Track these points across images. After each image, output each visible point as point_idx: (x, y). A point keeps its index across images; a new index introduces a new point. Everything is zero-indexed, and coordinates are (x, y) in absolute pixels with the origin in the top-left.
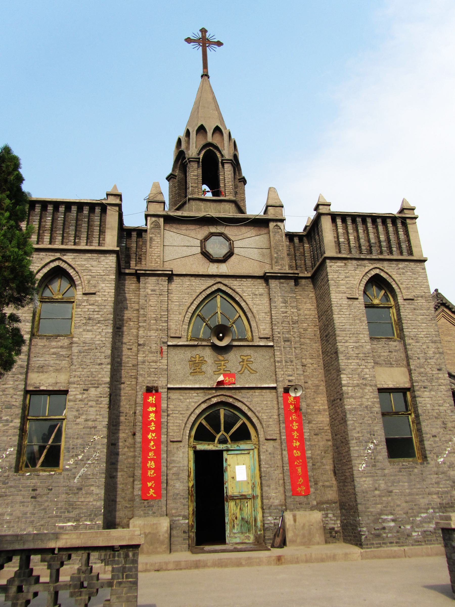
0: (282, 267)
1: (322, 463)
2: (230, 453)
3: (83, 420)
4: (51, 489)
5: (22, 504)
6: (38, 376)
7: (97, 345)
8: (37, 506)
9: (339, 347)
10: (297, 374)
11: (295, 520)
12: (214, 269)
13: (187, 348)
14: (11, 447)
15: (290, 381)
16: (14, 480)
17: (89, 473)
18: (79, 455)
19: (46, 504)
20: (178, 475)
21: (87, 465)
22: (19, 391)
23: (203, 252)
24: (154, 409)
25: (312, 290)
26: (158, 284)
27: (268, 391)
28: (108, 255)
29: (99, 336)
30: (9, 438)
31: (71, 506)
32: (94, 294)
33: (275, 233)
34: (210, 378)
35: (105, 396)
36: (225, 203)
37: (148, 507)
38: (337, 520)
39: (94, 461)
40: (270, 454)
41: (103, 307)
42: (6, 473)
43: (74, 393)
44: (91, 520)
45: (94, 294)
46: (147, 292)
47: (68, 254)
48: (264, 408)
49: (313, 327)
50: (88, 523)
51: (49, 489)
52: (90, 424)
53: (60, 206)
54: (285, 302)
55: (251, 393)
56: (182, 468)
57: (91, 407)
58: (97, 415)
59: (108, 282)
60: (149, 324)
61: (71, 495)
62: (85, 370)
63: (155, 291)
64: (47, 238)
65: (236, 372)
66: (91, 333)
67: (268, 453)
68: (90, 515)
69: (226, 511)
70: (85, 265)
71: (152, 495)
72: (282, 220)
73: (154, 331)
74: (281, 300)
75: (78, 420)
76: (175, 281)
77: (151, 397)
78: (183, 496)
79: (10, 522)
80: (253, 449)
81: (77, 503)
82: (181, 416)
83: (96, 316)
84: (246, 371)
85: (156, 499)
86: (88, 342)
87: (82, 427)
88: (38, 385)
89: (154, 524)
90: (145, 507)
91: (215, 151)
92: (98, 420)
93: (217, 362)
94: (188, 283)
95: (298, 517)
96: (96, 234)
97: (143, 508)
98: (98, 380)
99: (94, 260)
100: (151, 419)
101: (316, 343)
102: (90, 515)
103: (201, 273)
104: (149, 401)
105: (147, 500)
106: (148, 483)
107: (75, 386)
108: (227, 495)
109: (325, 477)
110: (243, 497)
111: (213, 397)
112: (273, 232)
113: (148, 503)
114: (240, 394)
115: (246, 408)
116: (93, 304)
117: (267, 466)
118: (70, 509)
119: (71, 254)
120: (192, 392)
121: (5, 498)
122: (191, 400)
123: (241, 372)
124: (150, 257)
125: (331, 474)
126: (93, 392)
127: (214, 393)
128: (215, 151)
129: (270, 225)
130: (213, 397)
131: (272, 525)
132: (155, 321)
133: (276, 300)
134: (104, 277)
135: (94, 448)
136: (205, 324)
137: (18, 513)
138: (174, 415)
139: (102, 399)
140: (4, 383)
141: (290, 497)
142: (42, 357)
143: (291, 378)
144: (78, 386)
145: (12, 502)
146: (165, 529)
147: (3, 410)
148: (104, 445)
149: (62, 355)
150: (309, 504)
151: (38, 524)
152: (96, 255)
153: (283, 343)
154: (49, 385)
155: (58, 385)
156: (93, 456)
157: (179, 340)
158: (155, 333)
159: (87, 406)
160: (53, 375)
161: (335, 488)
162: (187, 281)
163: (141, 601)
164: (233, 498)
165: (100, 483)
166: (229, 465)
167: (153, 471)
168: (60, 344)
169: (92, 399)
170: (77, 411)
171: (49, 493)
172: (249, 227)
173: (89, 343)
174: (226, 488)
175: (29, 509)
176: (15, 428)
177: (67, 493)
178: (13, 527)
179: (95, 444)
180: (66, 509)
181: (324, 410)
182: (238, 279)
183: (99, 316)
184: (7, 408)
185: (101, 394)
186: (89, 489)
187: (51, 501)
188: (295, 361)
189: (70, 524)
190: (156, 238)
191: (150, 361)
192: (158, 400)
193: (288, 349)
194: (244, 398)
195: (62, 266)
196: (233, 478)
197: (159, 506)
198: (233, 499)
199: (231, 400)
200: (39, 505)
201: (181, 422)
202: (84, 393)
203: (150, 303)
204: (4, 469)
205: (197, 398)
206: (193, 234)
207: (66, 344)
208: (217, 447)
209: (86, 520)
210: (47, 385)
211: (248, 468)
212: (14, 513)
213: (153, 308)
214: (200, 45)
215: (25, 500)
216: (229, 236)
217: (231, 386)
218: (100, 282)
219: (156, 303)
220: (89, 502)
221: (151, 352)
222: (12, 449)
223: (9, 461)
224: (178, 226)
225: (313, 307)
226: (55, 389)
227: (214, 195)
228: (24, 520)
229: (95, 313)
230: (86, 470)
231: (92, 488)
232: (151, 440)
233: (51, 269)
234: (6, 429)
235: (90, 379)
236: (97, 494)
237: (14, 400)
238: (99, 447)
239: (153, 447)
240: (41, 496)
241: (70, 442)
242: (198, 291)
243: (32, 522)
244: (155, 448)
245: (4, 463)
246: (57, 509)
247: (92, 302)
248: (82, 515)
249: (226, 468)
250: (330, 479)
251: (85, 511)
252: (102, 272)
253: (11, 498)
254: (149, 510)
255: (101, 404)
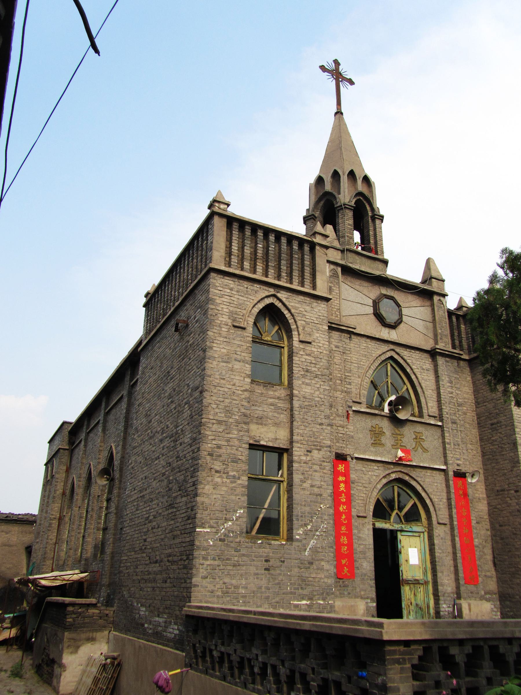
0: (446, 345)
1: (483, 552)
2: (403, 533)
3: (308, 486)
4: (283, 562)
5: (255, 577)
6: (258, 429)
7: (316, 402)
8: (271, 580)
9: (518, 439)
10: (464, 459)
11: (470, 610)
12: (385, 333)
13: (367, 416)
14: (241, 508)
15: (458, 465)
16: (246, 547)
17: (318, 546)
18: (309, 525)
19: (280, 578)
20: (365, 554)
21: (315, 537)
22: (244, 443)
23: (377, 313)
24: (344, 479)
25: (469, 374)
26: (341, 340)
27: (437, 472)
28: (319, 302)
29: (318, 393)
30: (238, 497)
31: (304, 582)
32: (310, 343)
33: (439, 307)
34: (389, 452)
35: (328, 460)
36: (379, 263)
37: (344, 587)
38: (498, 611)
39: (322, 533)
40: (442, 538)
41: (319, 360)
42: (237, 538)
43: (299, 453)
44: (324, 600)
45: (310, 343)
46: (331, 347)
47: (282, 292)
48: (436, 490)
49: (471, 412)
50: (322, 602)
51: (281, 561)
52: (316, 490)
53: (270, 234)
54: (451, 382)
55: (423, 473)
56: (367, 546)
57: (316, 471)
58: (321, 481)
59: (321, 332)
60: (335, 383)
61: (303, 570)
62: (307, 429)
63: (338, 348)
64: (260, 268)
65: (411, 448)
66: (309, 388)
67: (440, 537)
68: (323, 593)
69: (402, 595)
70: (299, 308)
71: (346, 574)
72: (444, 295)
73: (340, 393)
74: (447, 379)
75: (305, 485)
76: (353, 340)
77: (340, 466)
78: (369, 577)
79: (245, 597)
80: (423, 532)
81: (310, 579)
82: (364, 489)
83: (313, 369)
84: (419, 448)
85: (350, 578)
86: (308, 397)
87: (309, 493)
88: (258, 438)
89: (352, 606)
90: (340, 586)
91: (365, 202)
92: (323, 487)
93: (394, 436)
94: (365, 345)
95: (472, 606)
96: (307, 275)
97: (339, 588)
98: (320, 442)
99: (307, 304)
100: (342, 489)
101: (474, 429)
102: (323, 593)
103: (377, 337)
104: (339, 469)
105: (342, 579)
106: (342, 561)
107: (299, 445)
108: (402, 579)
109: (486, 567)
110: (416, 582)
111: (392, 473)
112: (437, 306)
113: (343, 582)
114: (415, 472)
115: (421, 488)
116: (309, 355)
117: (440, 551)
118: (303, 586)
119: (285, 293)
120: (373, 464)
121: (238, 568)
122: (372, 473)
123: (415, 449)
124: (331, 308)
125: (491, 564)
126: (315, 453)
127: (392, 468)
128: (365, 202)
129: (434, 298)
130: (392, 473)
131: (446, 613)
132: (340, 382)
133: (443, 378)
134: (318, 325)
135: (321, 518)
136: (377, 391)
137: (252, 587)
138: (359, 488)
139: (325, 464)
140: (228, 431)
141: (463, 585)
142: (260, 406)
143: (459, 462)
144: (302, 446)
145: (246, 573)
146: (362, 611)
147: (229, 464)
148: (330, 515)
149: (279, 408)
150: (478, 593)
151: (274, 601)
152: (308, 299)
153: (450, 425)
154: (269, 441)
155: (278, 441)
156: (321, 527)
157: (359, 405)
158: (341, 394)
159: (311, 470)
160: (273, 429)
161: (495, 579)
162: (364, 342)
163: (61, 692)
164: (407, 582)
165: (330, 558)
166: (403, 547)
167: (346, 547)
168: (277, 394)
169: (316, 463)
170: (303, 474)
171: (281, 565)
172: (415, 296)
173: (309, 399)
174: (402, 571)
175: (263, 583)
176: (243, 487)
177: (299, 567)
178: (249, 602)
179: (322, 514)
180: (299, 585)
181: (483, 499)
182: (408, 350)
183: (316, 370)
184: (233, 462)
185: (323, 458)
186: (319, 564)
187: (284, 575)
188: (462, 445)
189: (304, 602)
190: (334, 288)
191: (338, 425)
192: (347, 468)
193: (455, 431)
194: (418, 477)
195: (276, 304)
196: (407, 561)
197: (353, 587)
198: (408, 583)
199: (407, 478)
200: (272, 578)
201: (364, 495)
202: (307, 455)
203: (335, 360)
204: (235, 534)
205: (377, 471)
206: (365, 291)
207: (283, 395)
208: (393, 526)
209: (319, 599)
210: (267, 440)
211: (420, 551)
212: (249, 586)
213: (337, 366)
214: (333, 77)
215: (259, 572)
216: (399, 302)
217: (408, 463)
218: (314, 330)
219: (340, 361)
220: (321, 578)
221: (338, 415)
222: (242, 511)
223: (239, 525)
224: (353, 280)
225: (470, 391)
226: (275, 446)
227: (363, 249)
228: (259, 595)
229: (313, 365)
230: (315, 542)
231: (323, 563)
232: (343, 512)
233: (265, 306)
234: (234, 487)
235: (312, 439)
236: (328, 570)
237: (240, 453)
238: (326, 517)
239: (345, 521)
240: (274, 568)
241: (299, 508)
242: (374, 355)
243: (267, 598)
244: (346, 522)
245: (235, 527)
246: (291, 584)
247: (308, 352)
248: (315, 593)
249: (401, 550)
250: (490, 569)
251: (317, 588)
252: (315, 319)
253: (244, 568)
254: (344, 590)
255: (324, 469)
